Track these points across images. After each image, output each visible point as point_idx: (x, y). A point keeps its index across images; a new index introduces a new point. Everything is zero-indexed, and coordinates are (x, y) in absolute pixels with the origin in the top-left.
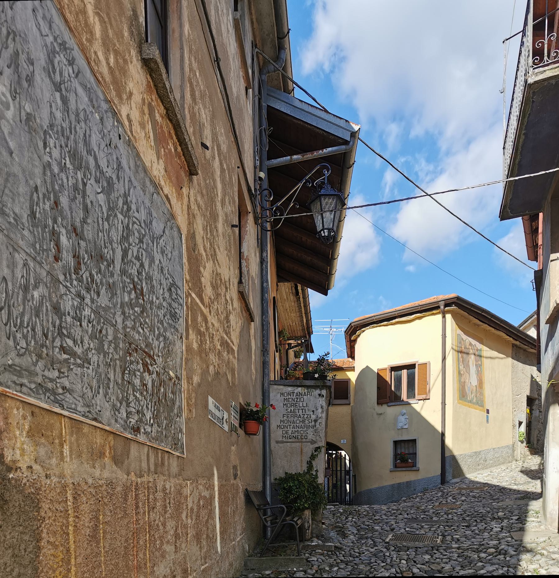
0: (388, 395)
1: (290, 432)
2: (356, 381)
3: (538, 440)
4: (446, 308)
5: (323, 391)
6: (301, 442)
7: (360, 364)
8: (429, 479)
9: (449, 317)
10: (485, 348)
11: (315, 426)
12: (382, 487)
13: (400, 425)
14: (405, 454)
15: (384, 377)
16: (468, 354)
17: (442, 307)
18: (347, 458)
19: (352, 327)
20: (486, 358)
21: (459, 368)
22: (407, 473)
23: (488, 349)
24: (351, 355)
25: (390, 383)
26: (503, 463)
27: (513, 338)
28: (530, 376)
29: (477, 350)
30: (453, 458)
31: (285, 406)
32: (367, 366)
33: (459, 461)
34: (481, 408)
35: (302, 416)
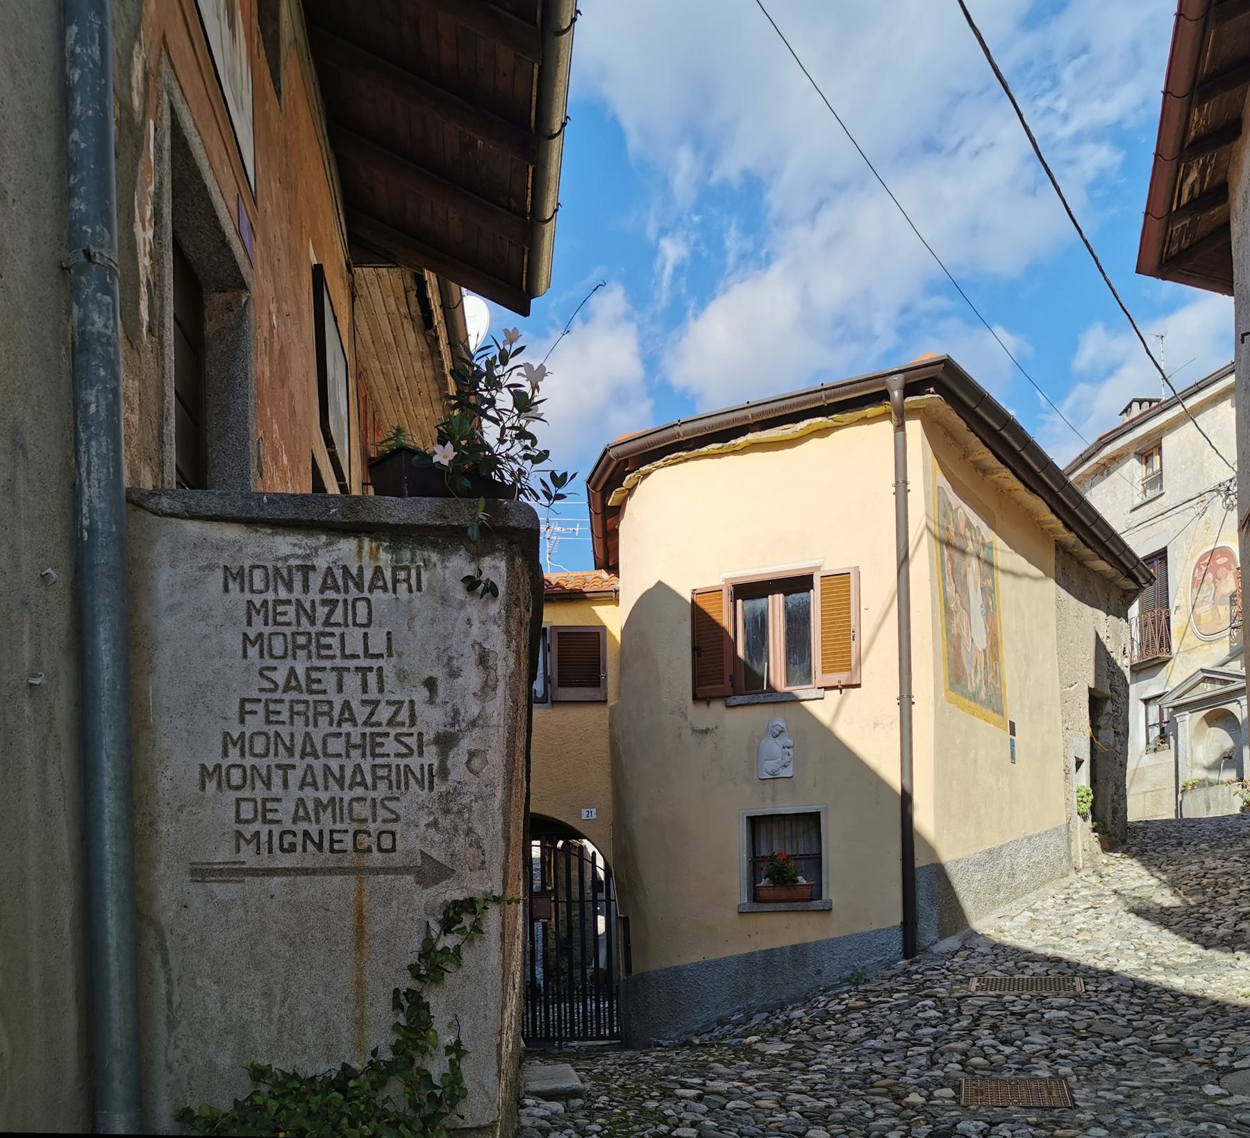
0: (728, 671)
1: (286, 809)
2: (623, 632)
3: (1115, 811)
4: (908, 399)
5: (487, 562)
6: (359, 871)
7: (634, 581)
8: (862, 939)
9: (914, 428)
10: (999, 543)
11: (444, 772)
12: (717, 963)
13: (769, 766)
14: (785, 859)
15: (715, 616)
16: (963, 552)
17: (896, 394)
18: (600, 862)
19: (610, 460)
20: (1005, 572)
21: (945, 591)
22: (793, 919)
23: (1007, 548)
24: (608, 560)
25: (732, 634)
26: (1050, 880)
27: (1065, 523)
28: (1094, 636)
29: (984, 545)
30: (939, 872)
31: (253, 652)
32: (660, 582)
33: (955, 881)
34: (995, 716)
35: (361, 713)
